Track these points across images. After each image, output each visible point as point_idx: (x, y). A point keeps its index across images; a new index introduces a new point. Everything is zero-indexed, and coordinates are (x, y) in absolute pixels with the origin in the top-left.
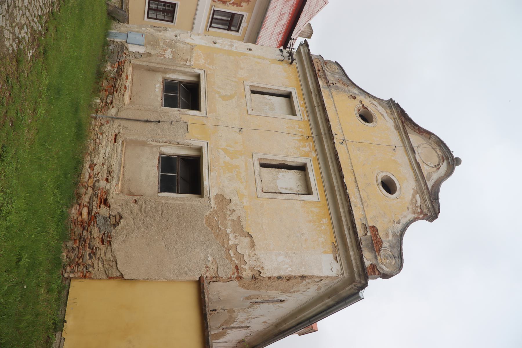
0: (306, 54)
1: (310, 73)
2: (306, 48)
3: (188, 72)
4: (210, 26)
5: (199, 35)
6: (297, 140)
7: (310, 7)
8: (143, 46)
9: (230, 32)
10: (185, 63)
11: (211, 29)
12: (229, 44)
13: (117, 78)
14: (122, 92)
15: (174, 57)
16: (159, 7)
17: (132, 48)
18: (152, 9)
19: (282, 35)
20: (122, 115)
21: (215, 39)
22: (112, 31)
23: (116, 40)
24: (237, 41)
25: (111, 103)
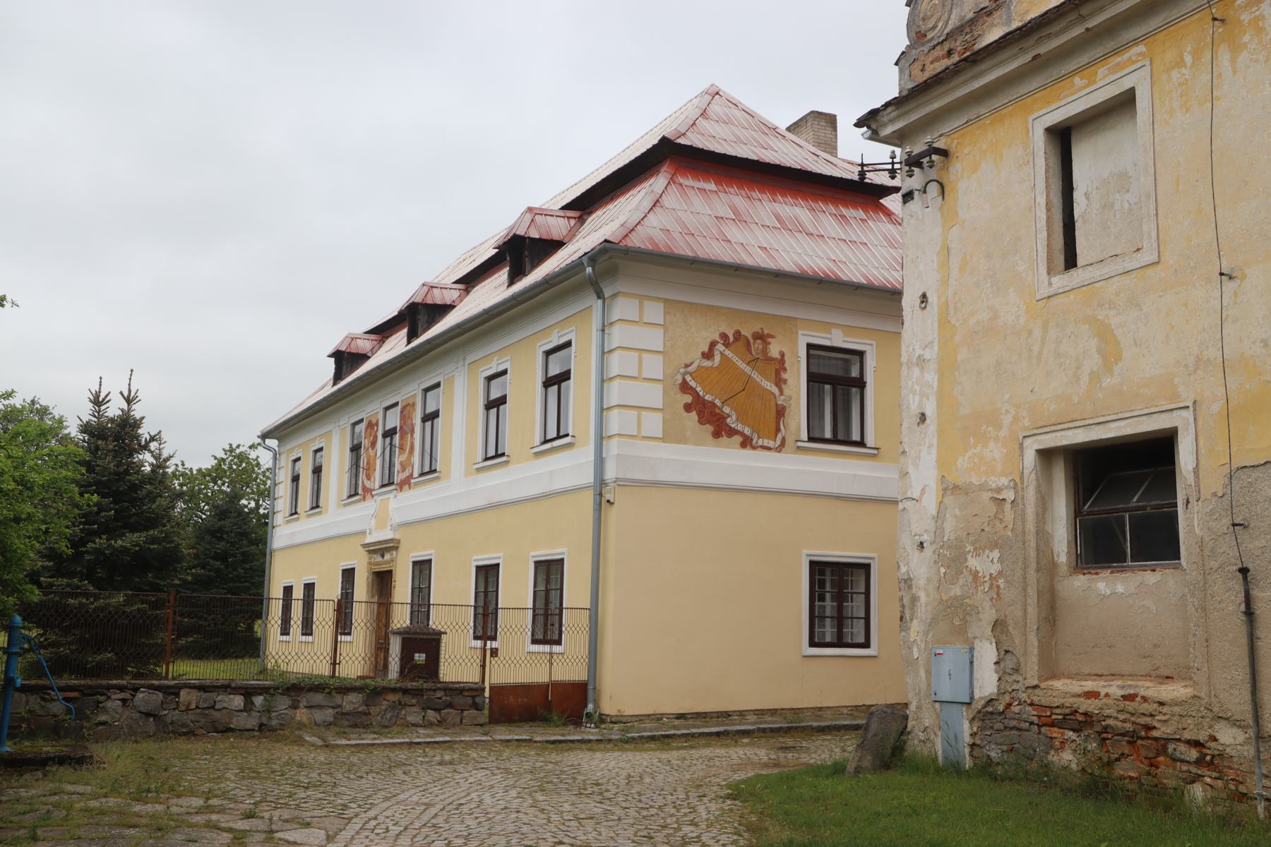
0: (901, 110)
1: (965, 82)
2: (884, 118)
3: (1038, 490)
4: (861, 444)
5: (904, 474)
6: (1233, 61)
7: (738, 141)
8: (972, 650)
9: (869, 378)
10: (1008, 506)
11: (870, 440)
12: (916, 371)
13: (1099, 729)
14: (1146, 707)
15: (994, 545)
16: (828, 613)
17: (987, 684)
18: (840, 634)
19: (844, 211)
20: (1239, 702)
21: (909, 422)
22: (940, 753)
23: (967, 739)
24: (904, 348)
25: (1197, 744)
